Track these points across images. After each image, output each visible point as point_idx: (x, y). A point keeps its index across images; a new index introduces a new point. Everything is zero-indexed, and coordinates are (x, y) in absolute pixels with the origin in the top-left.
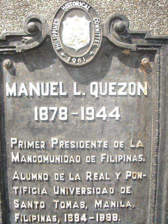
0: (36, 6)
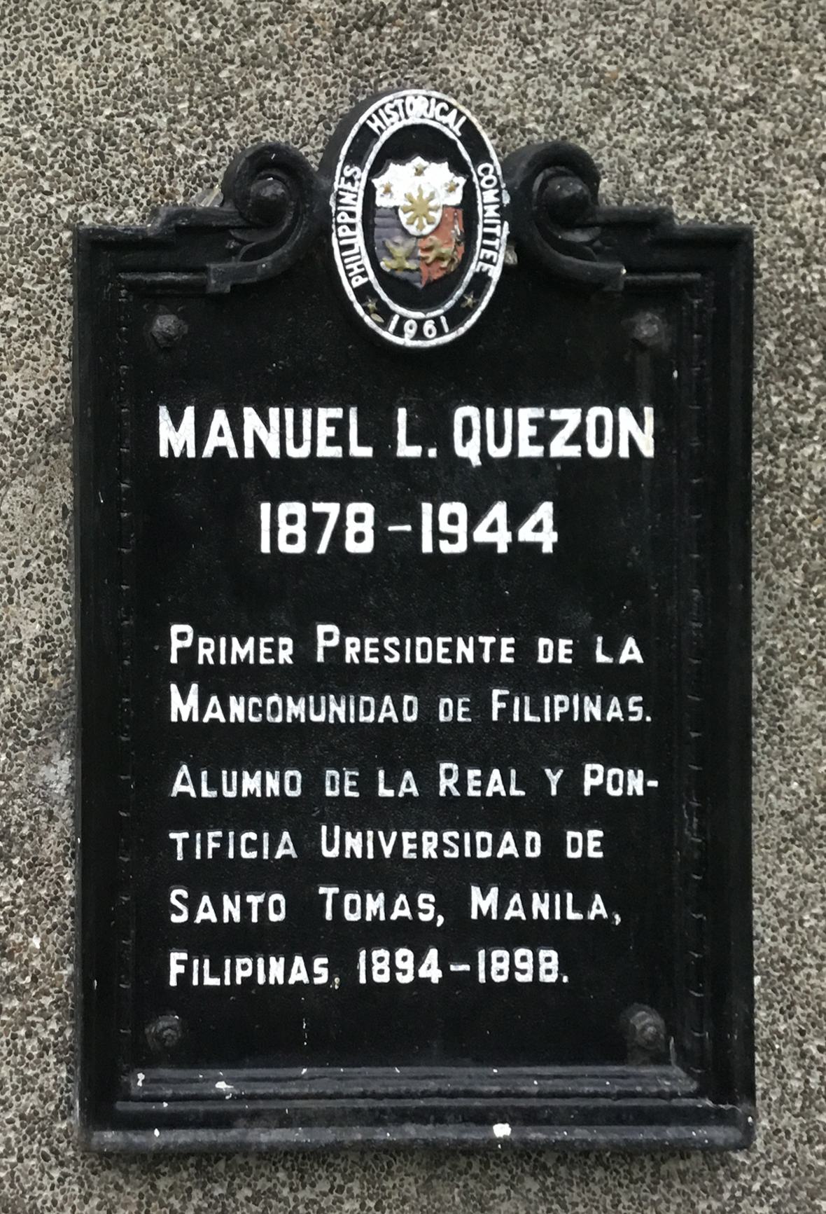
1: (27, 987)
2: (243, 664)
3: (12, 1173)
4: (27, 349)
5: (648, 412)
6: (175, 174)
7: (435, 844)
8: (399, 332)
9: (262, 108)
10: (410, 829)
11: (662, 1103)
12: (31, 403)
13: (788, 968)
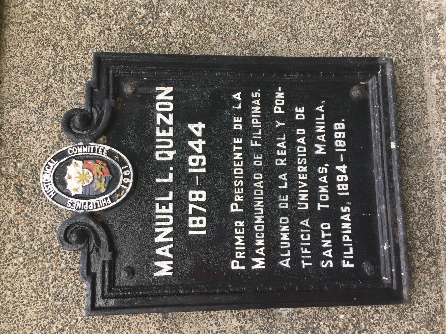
0: (46, 236)
1: (357, 319)
2: (244, 240)
3: (418, 322)
4: (134, 328)
5: (158, 89)
6: (72, 268)
7: (302, 167)
8: (127, 185)
9: (49, 233)
10: (298, 176)
11: (380, 89)
12: (154, 325)
13: (336, 42)
